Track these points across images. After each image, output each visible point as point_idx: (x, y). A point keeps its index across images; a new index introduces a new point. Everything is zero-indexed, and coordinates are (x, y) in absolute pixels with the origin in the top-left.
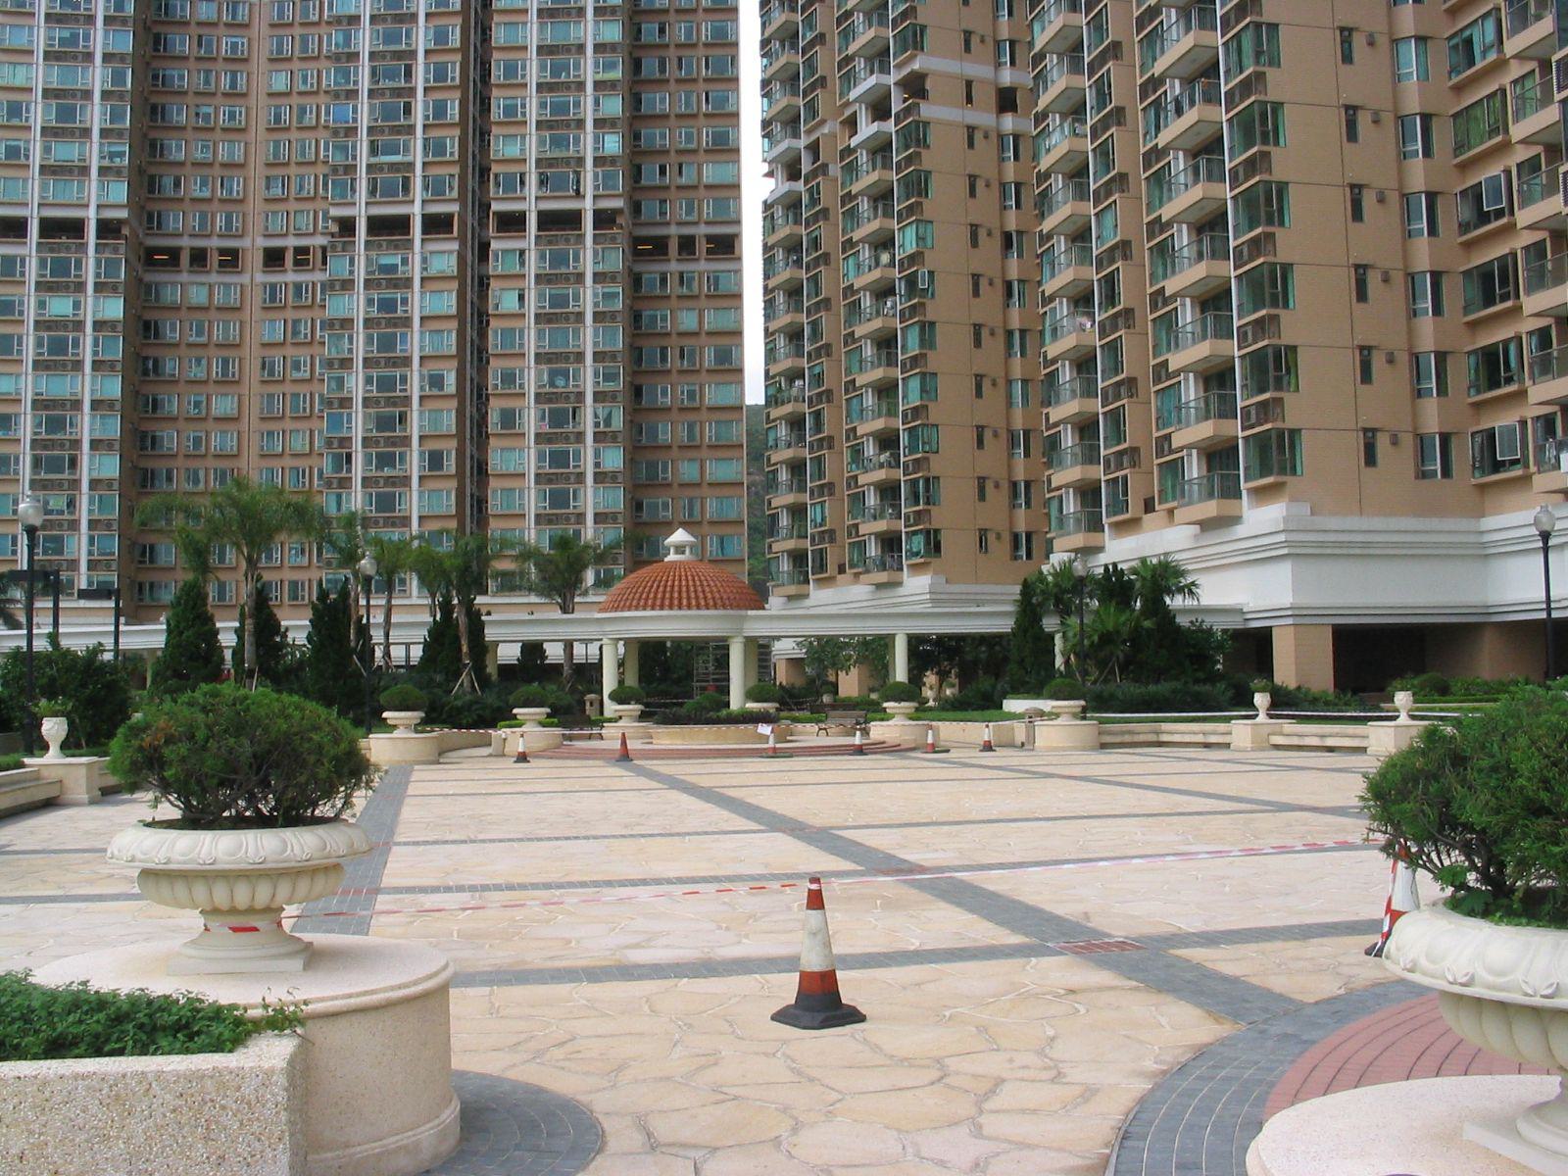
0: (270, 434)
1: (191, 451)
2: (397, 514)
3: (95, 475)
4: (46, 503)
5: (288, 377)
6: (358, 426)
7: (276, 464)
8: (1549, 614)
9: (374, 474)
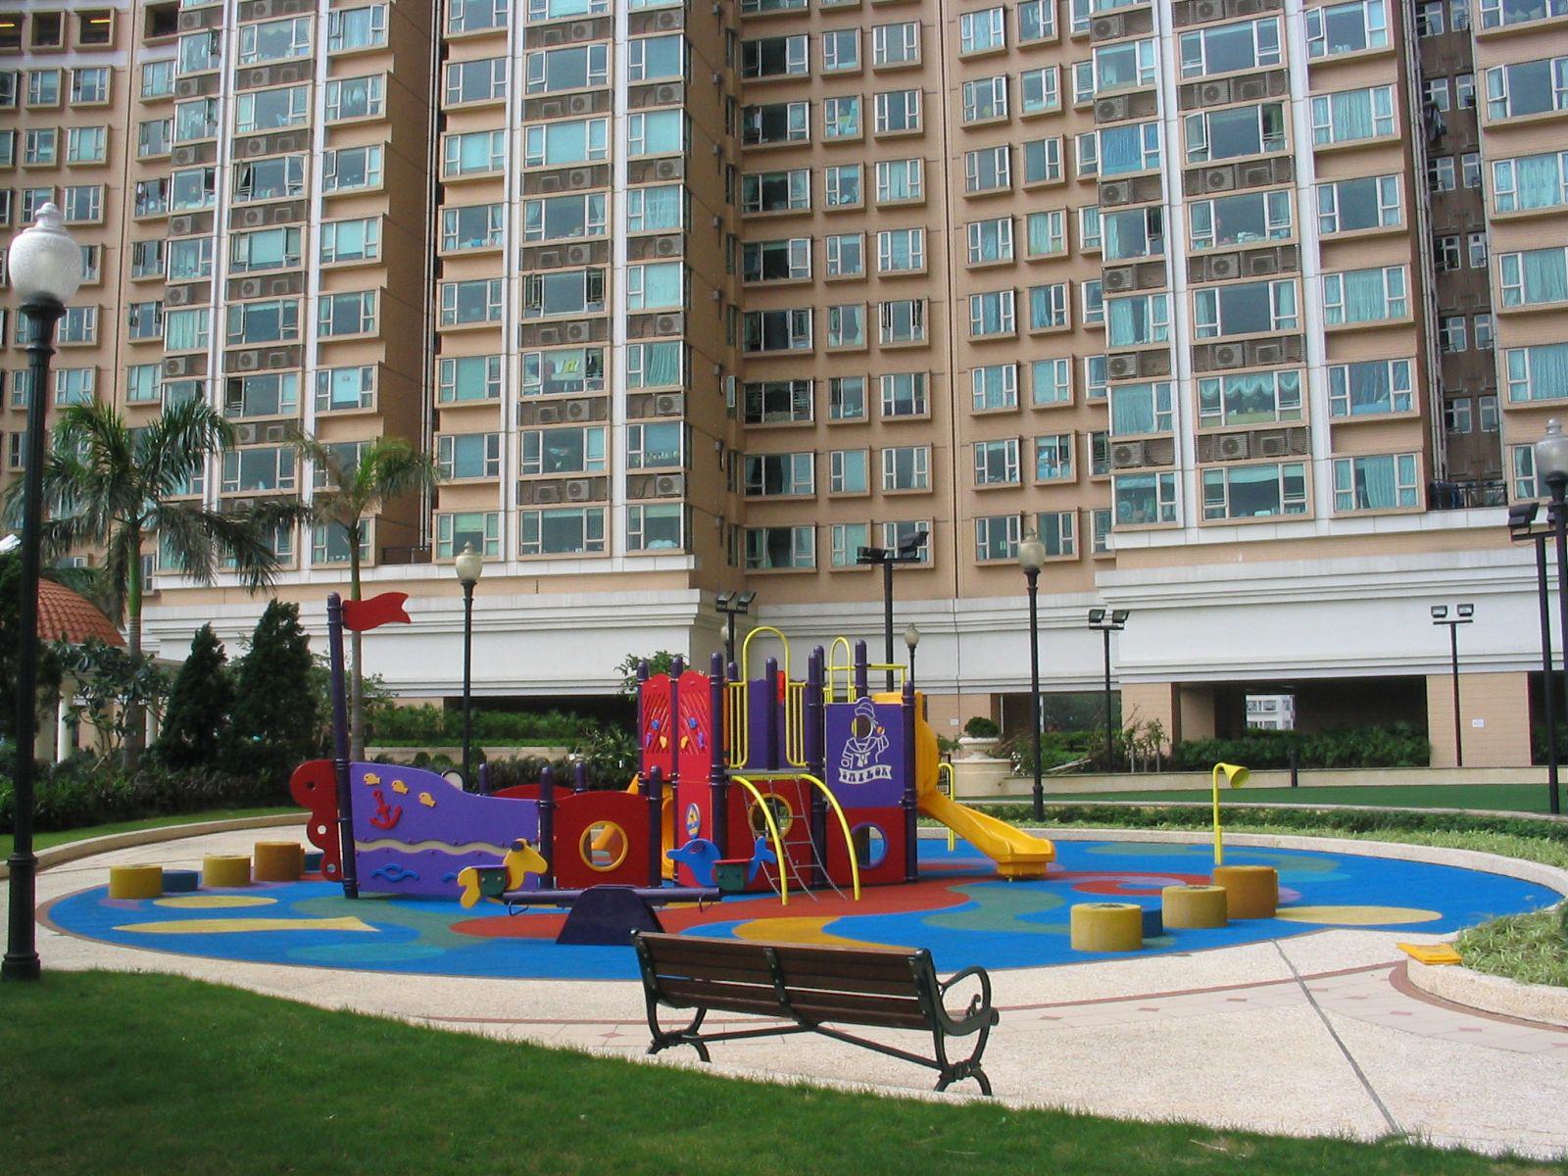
0: (990, 226)
1: (839, 273)
2: (1273, 332)
3: (638, 307)
4: (550, 368)
5: (1018, 113)
6: (1171, 147)
7: (1002, 282)
8: (1108, 687)
9: (1214, 248)
